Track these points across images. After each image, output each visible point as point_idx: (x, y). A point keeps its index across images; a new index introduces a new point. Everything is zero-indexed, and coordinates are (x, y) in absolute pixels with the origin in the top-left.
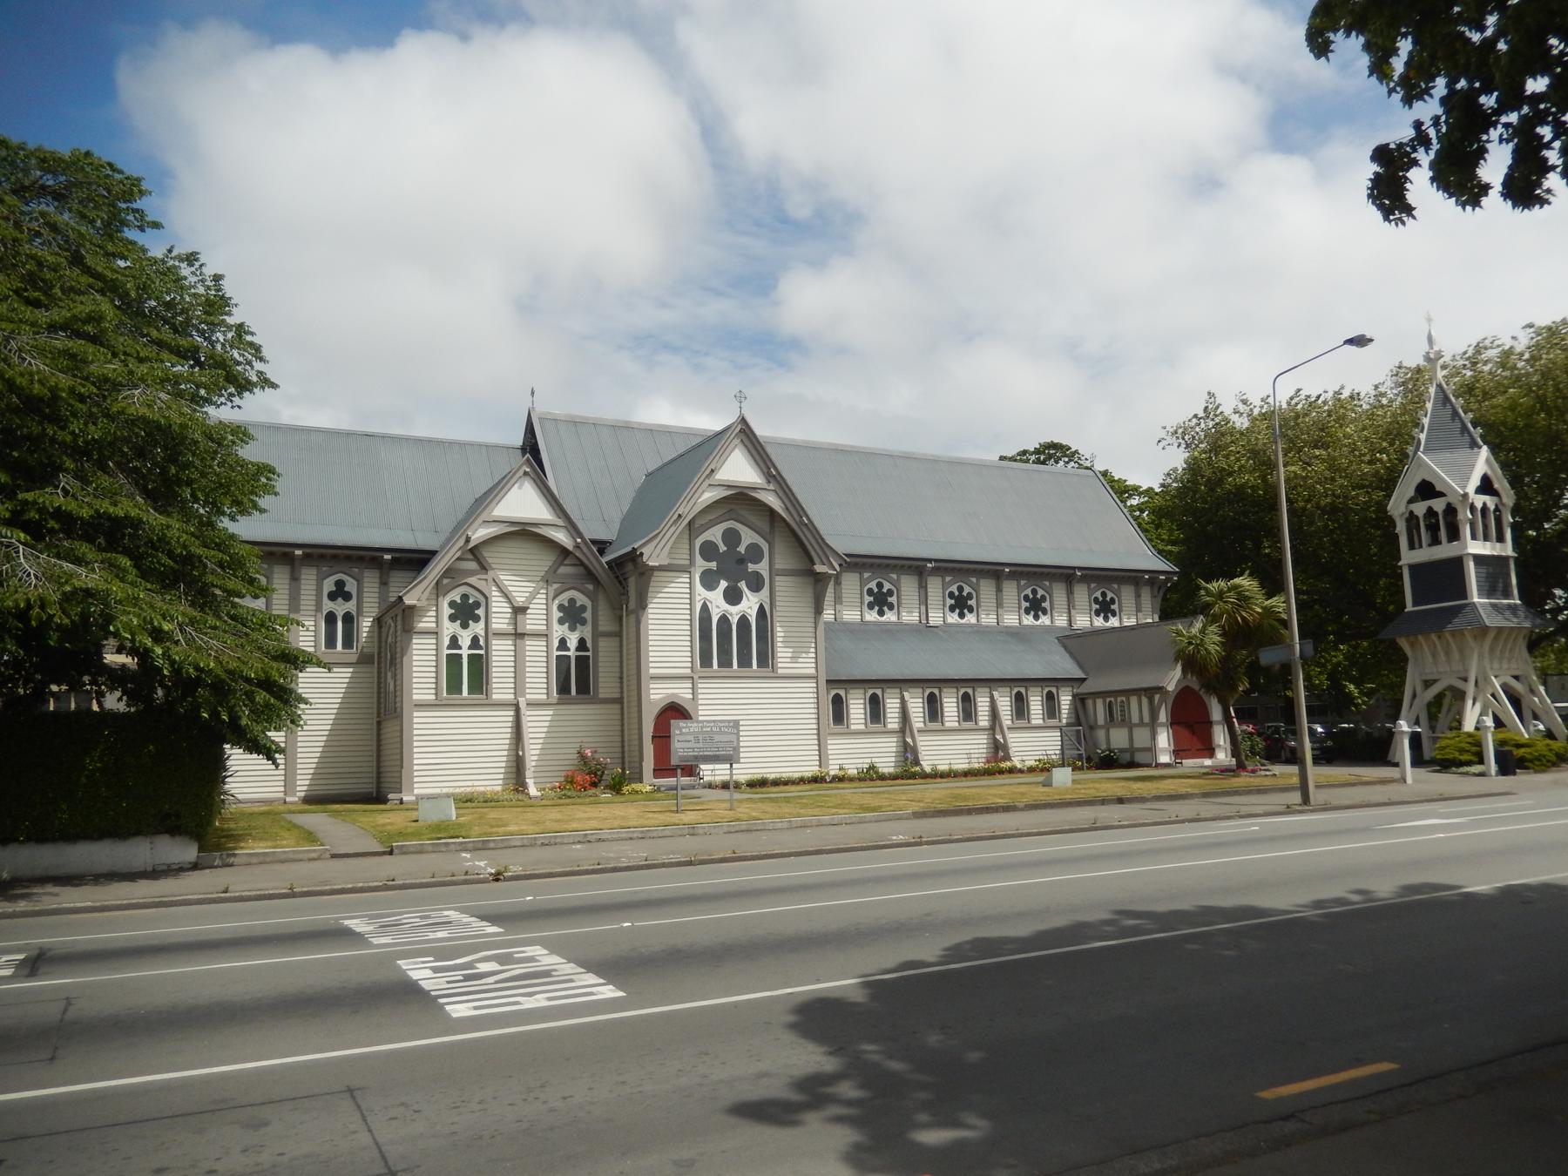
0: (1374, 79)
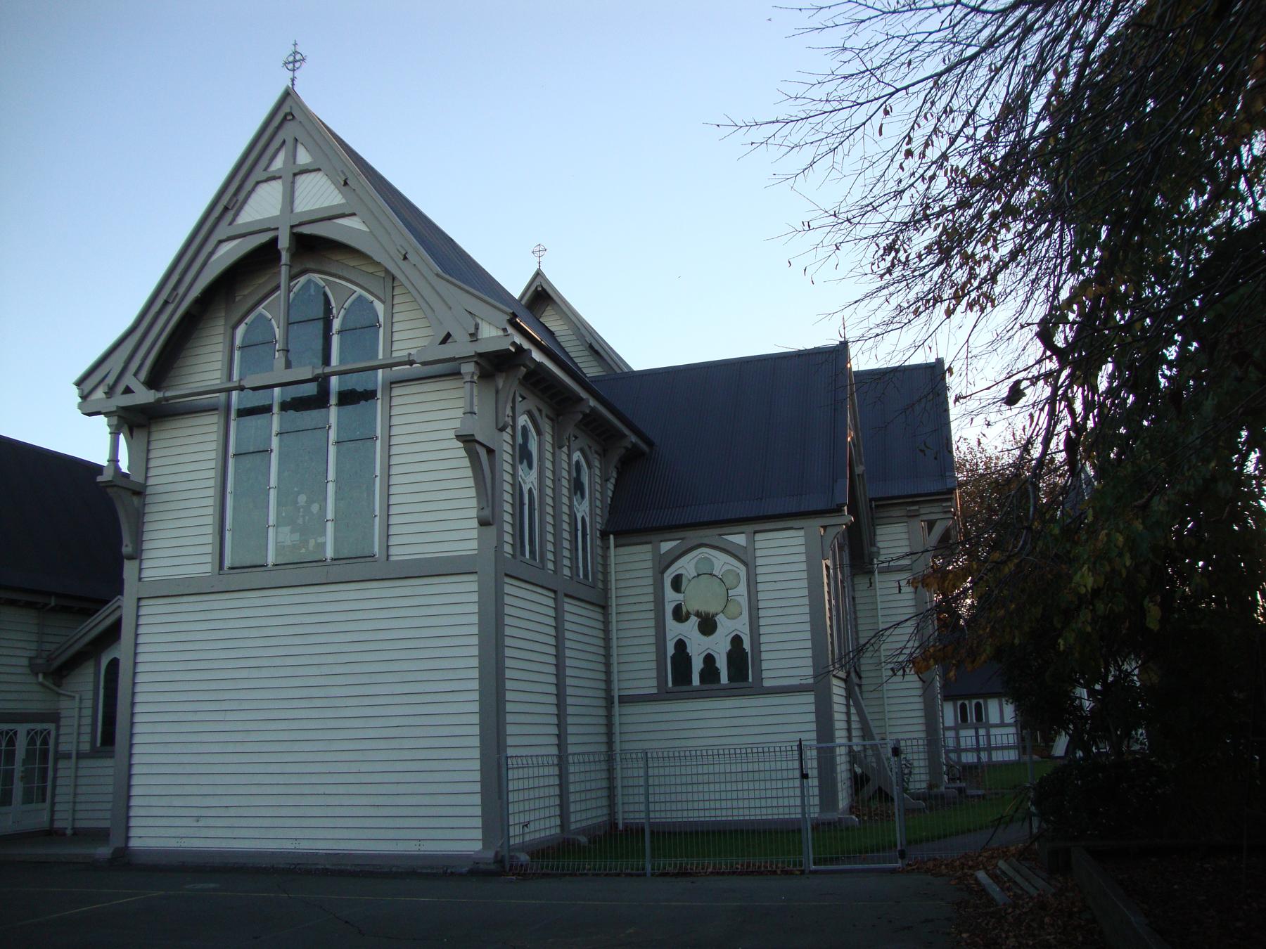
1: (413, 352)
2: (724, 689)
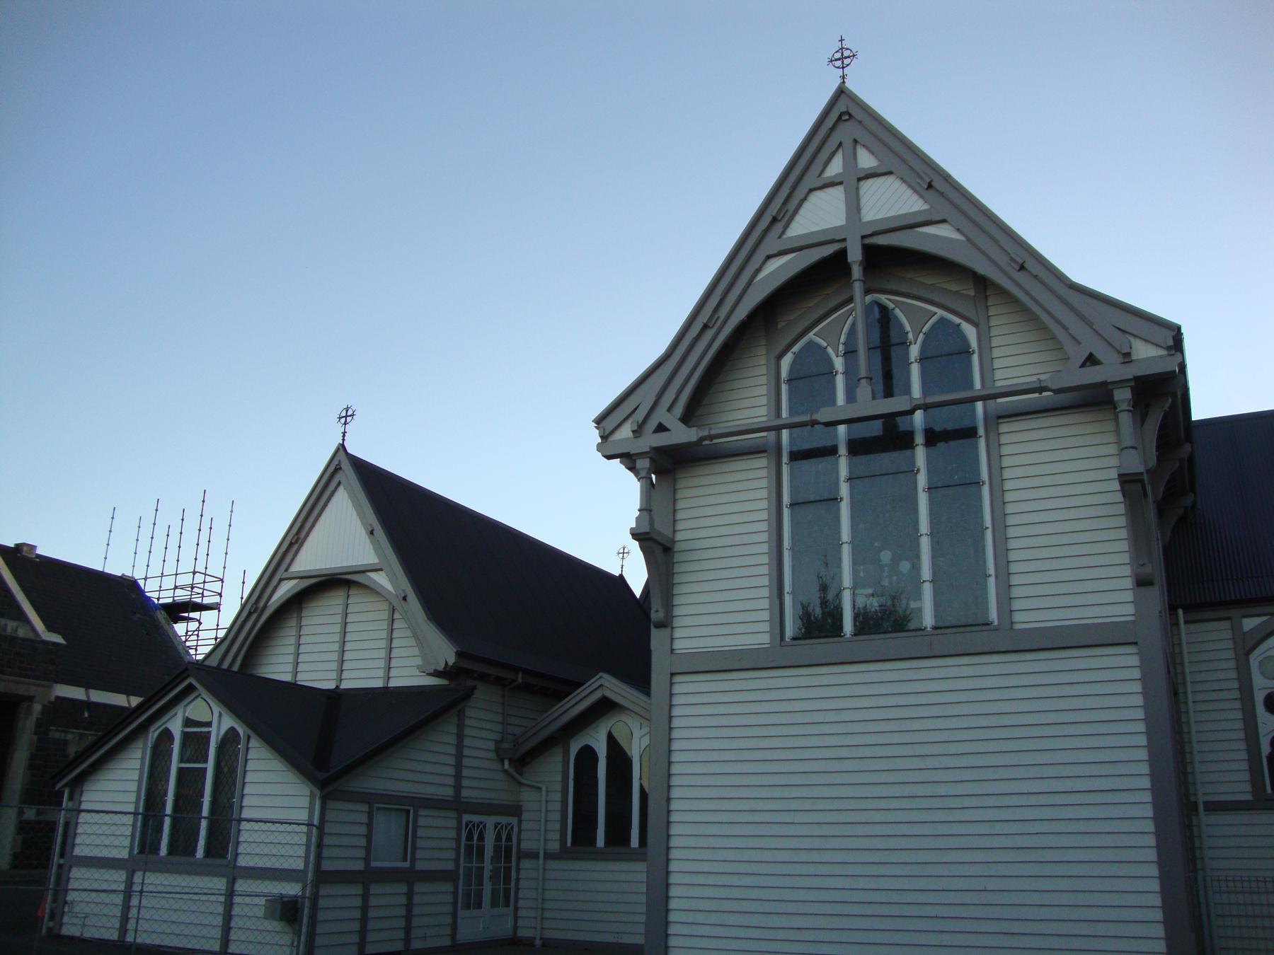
1: (1043, 377)
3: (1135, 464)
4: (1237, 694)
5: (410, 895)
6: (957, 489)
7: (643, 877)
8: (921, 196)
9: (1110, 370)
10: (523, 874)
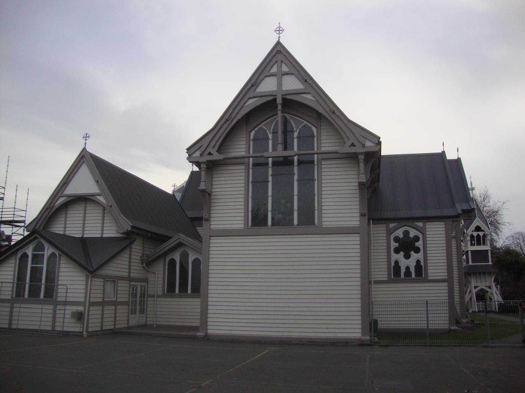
0: (451, 156)
2: (413, 279)
3: (364, 180)
4: (386, 247)
5: (116, 310)
6: (307, 182)
7: (199, 303)
8: (302, 83)
9: (358, 149)
10: (149, 303)
